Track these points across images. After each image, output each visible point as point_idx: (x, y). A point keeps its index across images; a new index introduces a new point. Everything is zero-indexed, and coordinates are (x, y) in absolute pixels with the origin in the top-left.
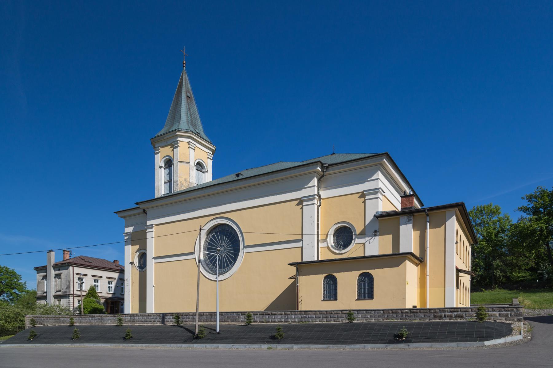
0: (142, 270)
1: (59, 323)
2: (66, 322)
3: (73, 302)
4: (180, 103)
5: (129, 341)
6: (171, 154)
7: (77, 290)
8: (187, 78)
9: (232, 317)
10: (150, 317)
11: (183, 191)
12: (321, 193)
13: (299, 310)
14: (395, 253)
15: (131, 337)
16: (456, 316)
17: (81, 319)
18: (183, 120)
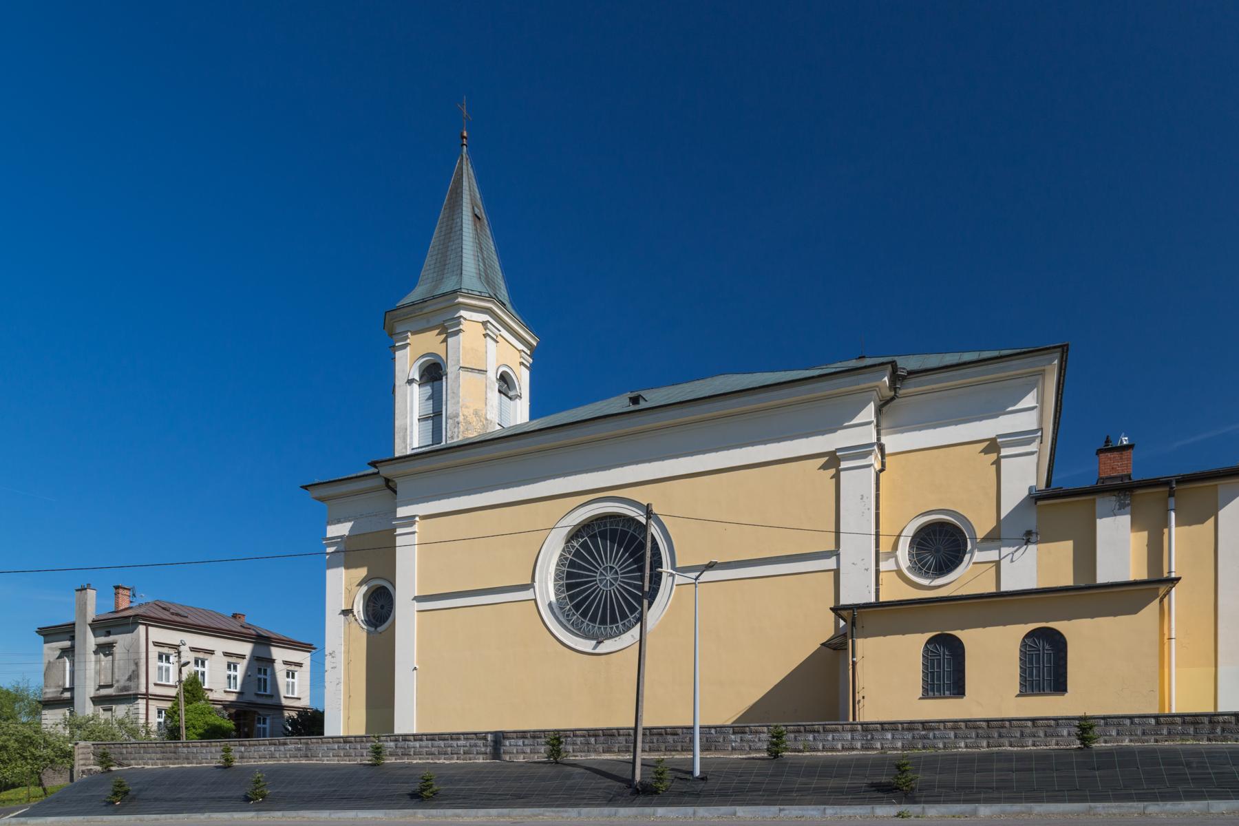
0: (376, 628)
1: (177, 761)
2: (196, 758)
3: (145, 712)
6: (441, 350)
7: (156, 685)
8: (471, 171)
10: (454, 743)
12: (884, 440)
13: (857, 720)
17: (243, 749)
18: (468, 269)
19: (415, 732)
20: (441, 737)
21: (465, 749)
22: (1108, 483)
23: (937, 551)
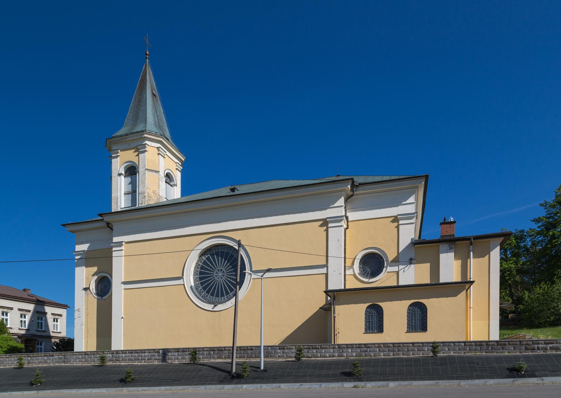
0: (102, 297)
4: (144, 100)
5: (133, 384)
6: (135, 160)
8: (151, 72)
10: (143, 355)
11: (151, 206)
12: (348, 214)
13: (336, 343)
15: (133, 380)
16: (551, 348)
17: (29, 358)
20: (136, 351)
22: (445, 238)
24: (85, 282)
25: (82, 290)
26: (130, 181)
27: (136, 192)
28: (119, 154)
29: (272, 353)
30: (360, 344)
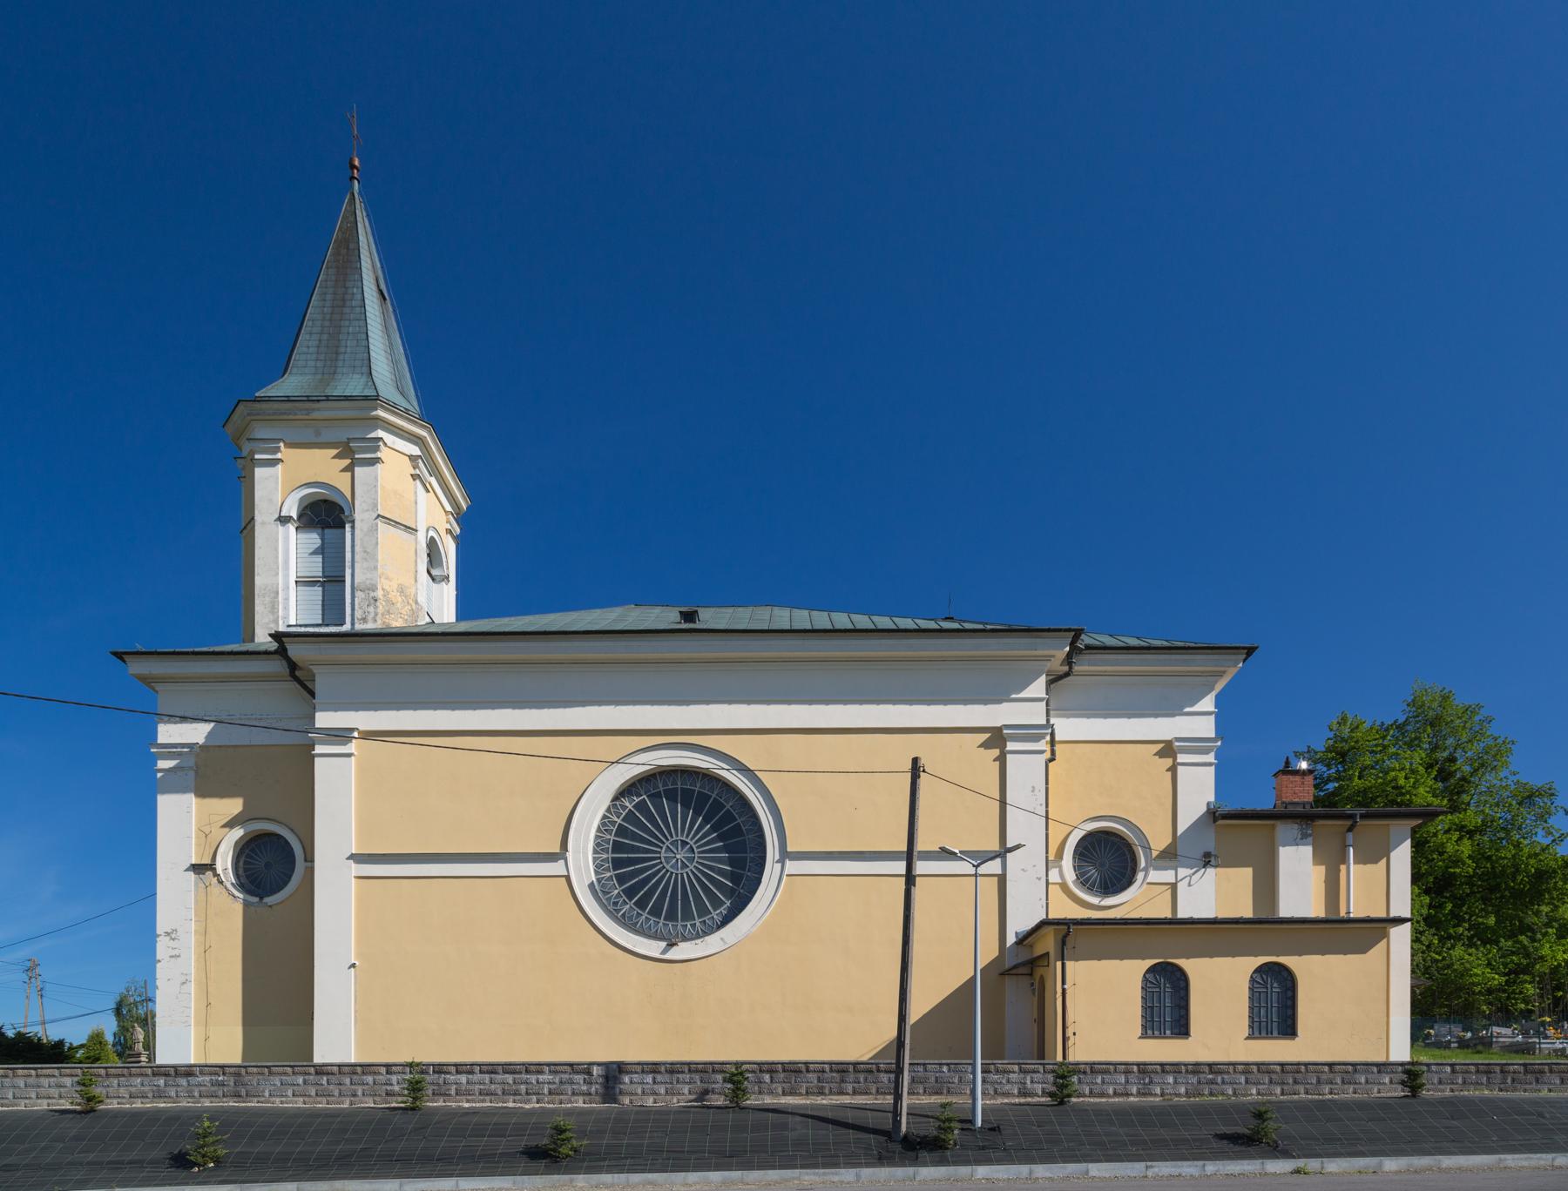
0: (261, 898)
6: (342, 482)
9: (933, 1079)
10: (533, 1078)
11: (394, 630)
14: (1263, 916)
19: (353, 1061)
20: (508, 1068)
21: (551, 1086)
22: (1290, 808)
23: (1102, 865)
24: (196, 845)
25: (186, 870)
26: (316, 546)
27: (344, 581)
28: (279, 456)
29: (953, 1083)
30: (1197, 1064)
